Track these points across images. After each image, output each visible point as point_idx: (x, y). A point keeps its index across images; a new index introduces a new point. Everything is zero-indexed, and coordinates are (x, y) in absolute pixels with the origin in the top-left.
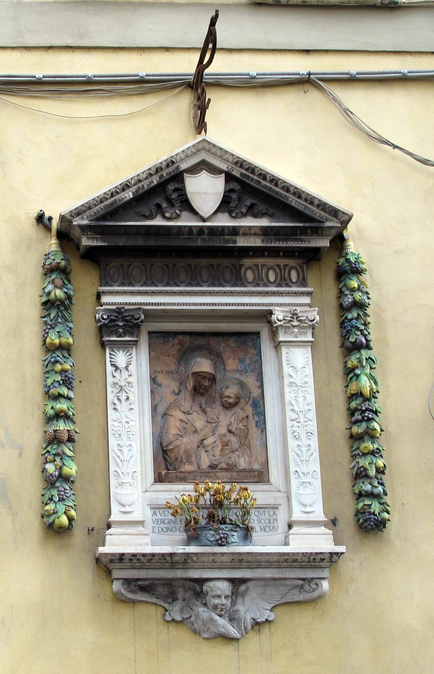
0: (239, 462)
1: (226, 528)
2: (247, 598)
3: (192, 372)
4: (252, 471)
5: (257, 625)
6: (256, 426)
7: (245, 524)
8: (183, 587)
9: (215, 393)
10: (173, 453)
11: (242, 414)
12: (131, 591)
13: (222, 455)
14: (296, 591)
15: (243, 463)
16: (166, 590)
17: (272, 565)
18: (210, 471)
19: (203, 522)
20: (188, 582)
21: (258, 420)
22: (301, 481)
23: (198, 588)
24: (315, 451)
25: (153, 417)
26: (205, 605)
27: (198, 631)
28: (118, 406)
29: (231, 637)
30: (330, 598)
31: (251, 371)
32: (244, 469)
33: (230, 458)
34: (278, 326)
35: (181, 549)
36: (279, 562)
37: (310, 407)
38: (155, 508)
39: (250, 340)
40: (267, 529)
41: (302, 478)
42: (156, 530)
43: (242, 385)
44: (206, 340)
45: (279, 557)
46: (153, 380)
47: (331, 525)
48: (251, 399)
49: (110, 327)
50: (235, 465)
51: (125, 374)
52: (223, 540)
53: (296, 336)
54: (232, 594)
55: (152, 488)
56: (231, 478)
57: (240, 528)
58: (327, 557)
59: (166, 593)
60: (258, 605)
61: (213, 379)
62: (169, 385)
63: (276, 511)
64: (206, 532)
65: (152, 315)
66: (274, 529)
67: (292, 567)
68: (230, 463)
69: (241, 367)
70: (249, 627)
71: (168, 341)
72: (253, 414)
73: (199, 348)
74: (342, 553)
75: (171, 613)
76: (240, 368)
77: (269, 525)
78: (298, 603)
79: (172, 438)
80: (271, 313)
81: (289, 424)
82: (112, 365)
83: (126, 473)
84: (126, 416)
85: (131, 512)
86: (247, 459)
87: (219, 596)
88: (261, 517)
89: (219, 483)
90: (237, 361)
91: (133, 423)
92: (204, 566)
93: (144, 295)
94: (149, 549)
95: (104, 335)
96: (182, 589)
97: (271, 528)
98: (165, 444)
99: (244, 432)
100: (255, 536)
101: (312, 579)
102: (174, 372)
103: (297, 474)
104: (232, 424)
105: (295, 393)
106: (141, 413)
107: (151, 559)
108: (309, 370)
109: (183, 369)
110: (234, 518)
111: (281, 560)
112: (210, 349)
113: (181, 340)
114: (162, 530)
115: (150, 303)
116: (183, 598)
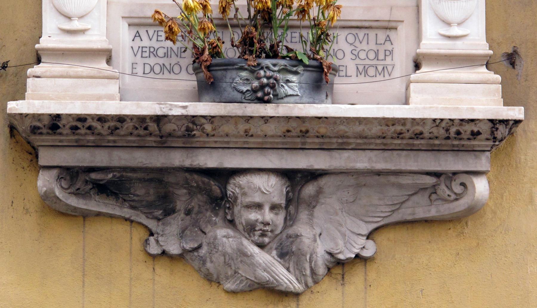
1: (275, 65)
2: (319, 212)
5: (338, 266)
7: (316, 59)
8: (187, 185)
12: (77, 194)
14: (421, 199)
16: (152, 191)
17: (370, 144)
19: (230, 53)
20: (196, 177)
23: (216, 189)
26: (232, 223)
27: (215, 276)
29: (283, 288)
30: (495, 213)
35: (177, 108)
36: (384, 138)
38: (137, 24)
40: (372, 71)
42: (139, 70)
45: (386, 128)
47: (506, 63)
52: (267, 89)
54: (289, 201)
57: (305, 66)
58: (485, 128)
59: (151, 198)
60: (341, 225)
63: (392, 34)
64: (233, 74)
66: (385, 71)
67: (412, 149)
70: (321, 270)
74: (517, 122)
75: (160, 239)
77: (375, 62)
78: (427, 222)
85: (83, 32)
87: (259, 206)
88: (360, 47)
92: (228, 142)
94: (112, 108)
96: (185, 191)
97: (380, 68)
100: (340, 84)
101: (455, 173)
107: (117, 128)
110: (299, 49)
111: (390, 134)
114: (152, 69)
116: (185, 210)
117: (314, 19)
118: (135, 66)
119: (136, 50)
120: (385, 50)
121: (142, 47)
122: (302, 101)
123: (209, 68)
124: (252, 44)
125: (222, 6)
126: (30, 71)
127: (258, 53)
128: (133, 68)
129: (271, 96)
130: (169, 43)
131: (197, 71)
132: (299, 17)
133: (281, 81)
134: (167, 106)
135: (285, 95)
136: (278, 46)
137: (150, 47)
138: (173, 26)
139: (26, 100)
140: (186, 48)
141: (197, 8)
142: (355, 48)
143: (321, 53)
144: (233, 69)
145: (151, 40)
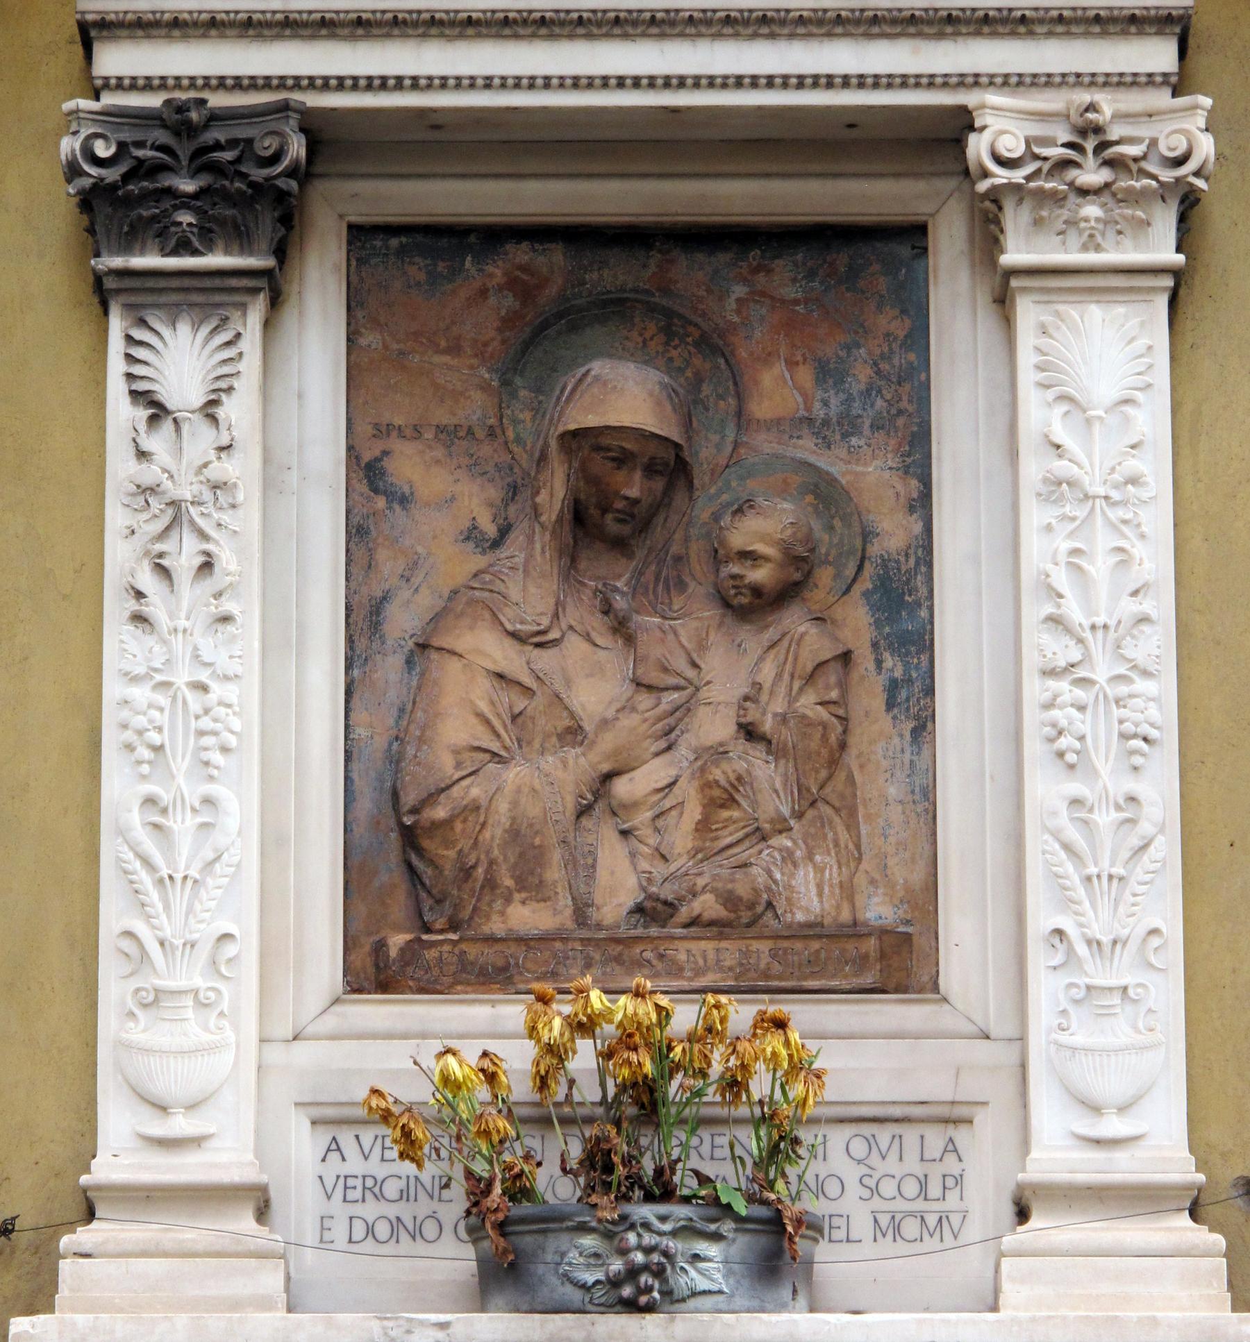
0: (789, 887)
1: (663, 1219)
3: (561, 429)
4: (855, 930)
6: (890, 705)
7: (764, 1202)
9: (687, 539)
10: (448, 844)
11: (815, 645)
13: (702, 854)
15: (808, 893)
18: (639, 931)
19: (556, 1187)
21: (898, 674)
22: (1083, 981)
24: (1162, 830)
25: (355, 658)
28: (156, 607)
31: (875, 427)
32: (809, 925)
33: (745, 865)
34: (995, 188)
37: (1146, 606)
38: (331, 1121)
39: (876, 267)
40: (911, 1228)
41: (1089, 967)
42: (339, 1232)
43: (826, 495)
44: (653, 268)
46: (367, 472)
48: (868, 570)
49: (129, 202)
50: (770, 905)
51: (200, 440)
52: (644, 1279)
53: (1091, 244)
55: (330, 1022)
56: (743, 969)
57: (739, 1219)
61: (671, 466)
62: (448, 496)
63: (961, 1136)
64: (563, 1241)
65: (335, 142)
68: (742, 890)
69: (826, 403)
71: (455, 272)
72: (875, 645)
73: (615, 306)
76: (819, 411)
77: (920, 1205)
79: (447, 765)
80: (962, 123)
81: (1034, 689)
82: (134, 394)
83: (179, 942)
84: (196, 656)
85: (196, 1142)
86: (833, 874)
88: (882, 1168)
89: (639, 994)
90: (805, 375)
91: (230, 692)
93: (313, 37)
95: (104, 252)
97: (932, 1220)
98: (410, 798)
99: (824, 737)
102: (480, 434)
103: (1061, 948)
104: (764, 697)
105: (1071, 535)
106: (280, 642)
108: (1153, 419)
109: (526, 416)
112: (669, 314)
113: (523, 268)
114: (370, 1231)
115: (341, 79)
117: (761, 1102)
118: (327, 1223)
119: (329, 1184)
120: (944, 1176)
121: (346, 1177)
122: (731, 1307)
123: (502, 1227)
124: (609, 1168)
125: (538, 1072)
126: (65, 1241)
127: (623, 1189)
128: (322, 1228)
129: (656, 1295)
130: (409, 1168)
131: (475, 1236)
132: (724, 1097)
133: (679, 1258)
134: (401, 1322)
135: (689, 1293)
136: (673, 1172)
137: (364, 1177)
138: (412, 1125)
139: (57, 1314)
140: (450, 1179)
141: (472, 1081)
142: (869, 1171)
143: (780, 1185)
144: (561, 1230)
145: (366, 1158)
